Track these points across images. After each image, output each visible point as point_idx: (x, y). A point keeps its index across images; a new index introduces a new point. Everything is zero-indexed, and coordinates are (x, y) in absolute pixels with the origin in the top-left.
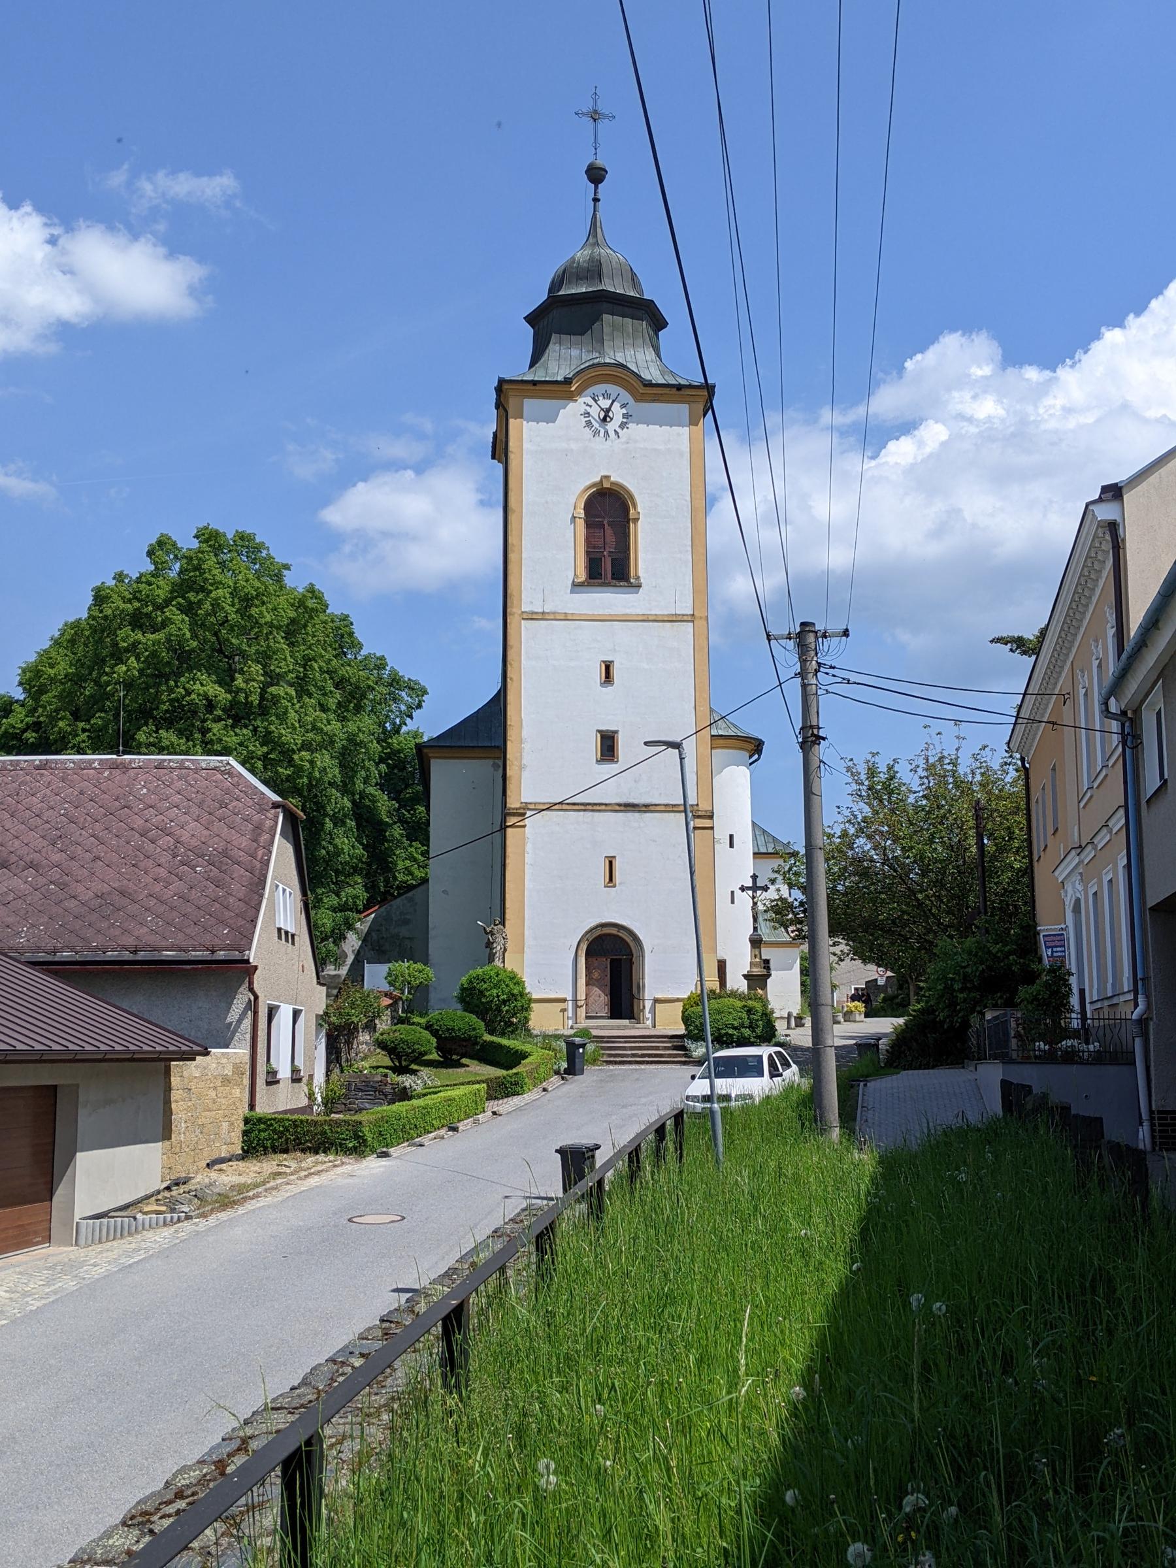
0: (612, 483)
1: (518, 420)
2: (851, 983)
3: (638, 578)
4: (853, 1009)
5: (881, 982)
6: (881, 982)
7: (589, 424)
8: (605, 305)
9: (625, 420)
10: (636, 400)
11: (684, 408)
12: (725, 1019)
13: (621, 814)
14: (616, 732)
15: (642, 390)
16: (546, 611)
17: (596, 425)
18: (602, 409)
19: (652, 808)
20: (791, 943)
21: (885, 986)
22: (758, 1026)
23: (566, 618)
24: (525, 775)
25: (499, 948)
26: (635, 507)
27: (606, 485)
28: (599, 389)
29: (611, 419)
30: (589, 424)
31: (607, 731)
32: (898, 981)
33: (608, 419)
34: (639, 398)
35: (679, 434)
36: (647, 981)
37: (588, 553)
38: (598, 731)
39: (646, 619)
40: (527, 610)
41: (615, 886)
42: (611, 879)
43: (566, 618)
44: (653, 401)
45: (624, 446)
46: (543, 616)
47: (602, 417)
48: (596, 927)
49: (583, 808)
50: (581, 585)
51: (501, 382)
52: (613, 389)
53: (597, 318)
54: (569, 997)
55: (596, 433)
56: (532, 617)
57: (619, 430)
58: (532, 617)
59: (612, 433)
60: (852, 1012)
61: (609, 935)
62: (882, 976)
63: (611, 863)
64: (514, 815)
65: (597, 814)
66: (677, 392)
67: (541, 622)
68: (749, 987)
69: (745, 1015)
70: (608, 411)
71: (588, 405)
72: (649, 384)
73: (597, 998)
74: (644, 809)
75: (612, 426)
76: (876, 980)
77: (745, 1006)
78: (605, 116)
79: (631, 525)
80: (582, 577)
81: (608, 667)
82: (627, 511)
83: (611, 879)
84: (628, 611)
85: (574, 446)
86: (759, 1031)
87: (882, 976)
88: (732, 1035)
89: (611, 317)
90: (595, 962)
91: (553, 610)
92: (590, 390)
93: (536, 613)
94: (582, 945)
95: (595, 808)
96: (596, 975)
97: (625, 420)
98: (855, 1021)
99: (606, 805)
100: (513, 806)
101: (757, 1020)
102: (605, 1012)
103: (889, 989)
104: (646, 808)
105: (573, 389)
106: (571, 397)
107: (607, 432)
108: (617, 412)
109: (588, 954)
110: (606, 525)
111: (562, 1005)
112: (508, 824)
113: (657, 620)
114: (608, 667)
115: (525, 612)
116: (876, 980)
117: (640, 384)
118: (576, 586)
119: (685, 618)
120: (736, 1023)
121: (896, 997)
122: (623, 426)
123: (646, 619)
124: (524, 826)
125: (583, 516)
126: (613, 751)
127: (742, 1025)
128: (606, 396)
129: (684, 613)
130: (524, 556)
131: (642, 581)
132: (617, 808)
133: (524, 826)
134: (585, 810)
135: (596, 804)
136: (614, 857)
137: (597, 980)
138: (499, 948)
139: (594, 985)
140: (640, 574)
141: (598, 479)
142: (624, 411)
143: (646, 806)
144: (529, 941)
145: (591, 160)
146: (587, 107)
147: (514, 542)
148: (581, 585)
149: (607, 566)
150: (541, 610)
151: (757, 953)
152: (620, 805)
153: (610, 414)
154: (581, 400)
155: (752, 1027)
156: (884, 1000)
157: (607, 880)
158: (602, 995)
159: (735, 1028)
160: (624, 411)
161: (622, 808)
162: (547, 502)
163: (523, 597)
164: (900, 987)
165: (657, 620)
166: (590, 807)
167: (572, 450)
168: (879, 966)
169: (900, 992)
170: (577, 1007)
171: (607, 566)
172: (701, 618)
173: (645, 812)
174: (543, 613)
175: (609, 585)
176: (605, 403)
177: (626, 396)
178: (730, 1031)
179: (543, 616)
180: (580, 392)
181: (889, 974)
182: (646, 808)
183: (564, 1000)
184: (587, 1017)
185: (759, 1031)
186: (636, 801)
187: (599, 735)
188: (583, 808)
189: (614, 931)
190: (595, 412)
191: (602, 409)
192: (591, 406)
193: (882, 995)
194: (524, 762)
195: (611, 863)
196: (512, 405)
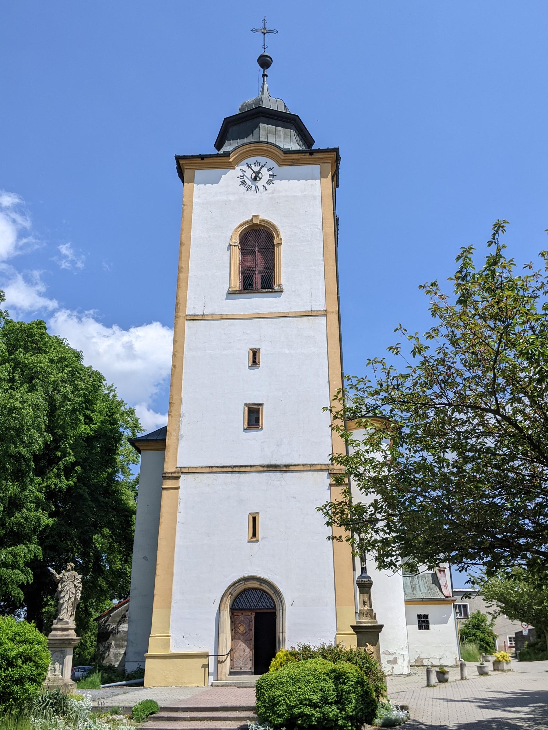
0: (260, 220)
1: (190, 184)
2: (506, 634)
3: (280, 285)
4: (501, 659)
5: (525, 633)
6: (525, 633)
7: (243, 183)
8: (262, 119)
9: (271, 179)
10: (280, 165)
11: (316, 168)
12: (301, 691)
13: (264, 474)
14: (261, 405)
15: (283, 156)
16: (205, 313)
17: (249, 183)
18: (254, 172)
19: (291, 468)
20: (444, 600)
21: (528, 636)
22: (350, 702)
23: (222, 318)
24: (182, 444)
25: (67, 597)
26: (278, 235)
27: (256, 222)
28: (251, 160)
29: (260, 179)
30: (243, 183)
31: (254, 404)
32: (537, 632)
33: (258, 179)
34: (282, 163)
35: (312, 185)
36: (286, 635)
37: (242, 272)
38: (246, 405)
39: (286, 316)
40: (190, 313)
41: (257, 541)
42: (254, 535)
43: (222, 318)
44: (292, 165)
45: (270, 196)
46: (203, 318)
47: (253, 177)
48: (239, 581)
49: (230, 470)
50: (234, 293)
51: (178, 158)
52: (262, 160)
53: (257, 126)
54: (212, 653)
55: (249, 188)
56: (194, 318)
57: (266, 185)
58: (194, 318)
59: (261, 188)
60: (499, 661)
61: (256, 589)
62: (525, 629)
63: (254, 519)
64: (169, 478)
65: (242, 475)
66: (310, 157)
67: (202, 322)
68: (360, 644)
69: (330, 685)
70: (259, 172)
71: (243, 171)
72: (287, 152)
73: (242, 653)
74: (285, 469)
75: (260, 184)
76: (522, 632)
77: (333, 671)
78: (269, 31)
79: (276, 249)
80: (237, 285)
81: (255, 354)
82: (272, 238)
83: (254, 535)
84: (272, 310)
85: (231, 198)
86: (350, 709)
87: (525, 629)
88: (309, 717)
89: (266, 125)
90: (240, 616)
91: (211, 312)
92: (247, 161)
93: (198, 315)
94: (225, 599)
95: (241, 469)
96: (241, 629)
97: (271, 179)
98: (503, 670)
99: (251, 466)
100: (169, 471)
101: (348, 692)
102: (249, 667)
103: (531, 638)
104: (286, 468)
105: (231, 160)
106: (230, 166)
107: (257, 187)
108: (265, 174)
109: (233, 610)
110: (257, 253)
111: (204, 661)
112: (163, 487)
113: (296, 316)
114: (255, 354)
115: (189, 315)
116: (522, 632)
117: (282, 153)
118: (231, 294)
119: (319, 313)
120: (315, 698)
121: (536, 644)
122: (269, 182)
123: (286, 316)
124: (178, 488)
125: (238, 244)
126: (259, 422)
127: (325, 700)
128: (257, 164)
129: (318, 309)
130: (190, 274)
131: (284, 287)
132: (261, 469)
133: (178, 488)
134: (232, 472)
135: (242, 466)
136: (258, 513)
137: (243, 635)
138: (67, 597)
139: (239, 639)
140: (282, 282)
141: (250, 218)
142: (271, 172)
143: (286, 466)
144: (176, 596)
145: (261, 52)
146: (260, 26)
147: (183, 266)
148: (234, 293)
149: (257, 281)
150: (202, 313)
151: (366, 599)
152: (263, 466)
153: (260, 175)
154: (238, 168)
155: (340, 702)
156: (529, 646)
157: (251, 535)
158: (247, 649)
159: (314, 706)
160: (271, 172)
161: (266, 469)
162: (209, 237)
163: (187, 303)
164: (539, 637)
165: (296, 316)
166: (236, 469)
167: (230, 201)
168: (522, 621)
169: (539, 640)
170: (219, 662)
171: (257, 281)
172: (332, 312)
173: (286, 471)
174: (203, 315)
175: (256, 292)
176: (256, 169)
177: (271, 163)
178: (308, 710)
179: (203, 318)
180: (238, 162)
181: (531, 627)
182: (286, 468)
183: (207, 656)
184: (231, 673)
185: (350, 709)
186: (278, 463)
187: (246, 408)
188: (230, 470)
189: (256, 585)
190: (249, 173)
191: (254, 172)
192: (245, 171)
193: (527, 643)
194: (181, 432)
195: (254, 519)
196: (187, 173)
